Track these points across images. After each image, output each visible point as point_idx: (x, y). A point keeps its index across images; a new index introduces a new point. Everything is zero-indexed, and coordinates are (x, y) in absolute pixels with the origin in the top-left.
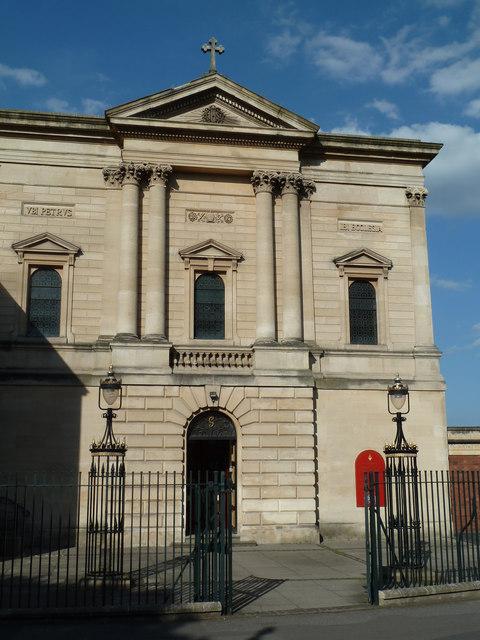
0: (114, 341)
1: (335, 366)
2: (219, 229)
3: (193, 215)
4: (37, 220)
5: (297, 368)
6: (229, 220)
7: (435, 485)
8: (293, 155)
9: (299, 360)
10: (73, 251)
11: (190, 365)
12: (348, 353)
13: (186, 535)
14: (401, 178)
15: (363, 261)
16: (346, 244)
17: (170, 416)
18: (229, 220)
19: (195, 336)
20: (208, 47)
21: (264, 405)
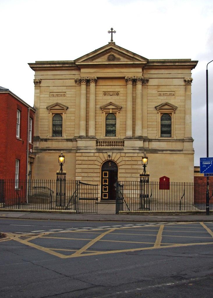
0: (78, 138)
1: (154, 145)
2: (114, 98)
3: (105, 94)
4: (162, 98)
6: (64, 95)
8: (140, 70)
9: (140, 144)
10: (65, 108)
12: (159, 140)
13: (24, 203)
14: (182, 75)
15: (57, 107)
16: (160, 100)
17: (96, 163)
18: (64, 95)
19: (106, 136)
21: (127, 159)
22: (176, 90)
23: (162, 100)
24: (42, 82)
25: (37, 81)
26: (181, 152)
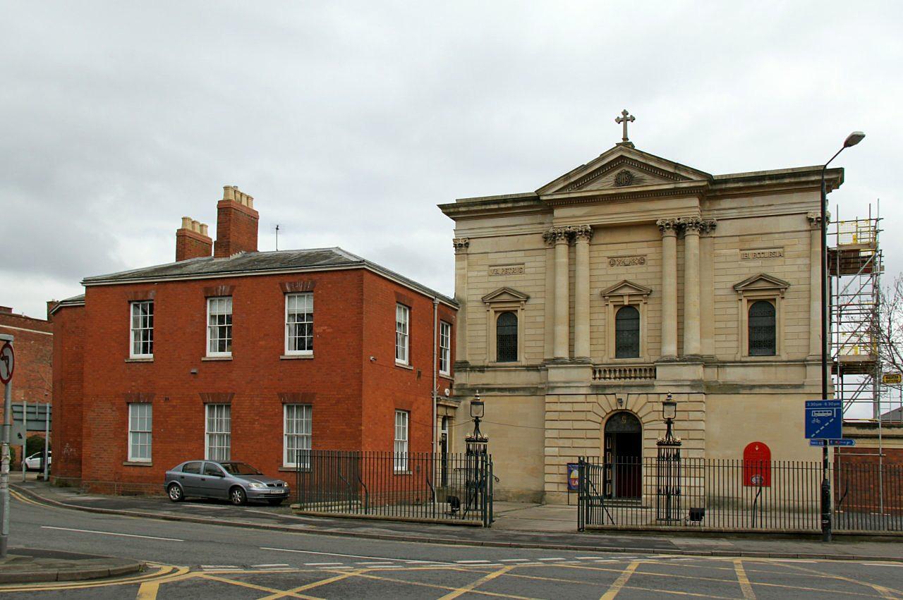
1: (733, 375)
3: (613, 261)
5: (691, 379)
7: (726, 469)
12: (743, 364)
15: (505, 297)
16: (746, 270)
17: (591, 416)
19: (617, 356)
23: (753, 268)
26: (800, 391)
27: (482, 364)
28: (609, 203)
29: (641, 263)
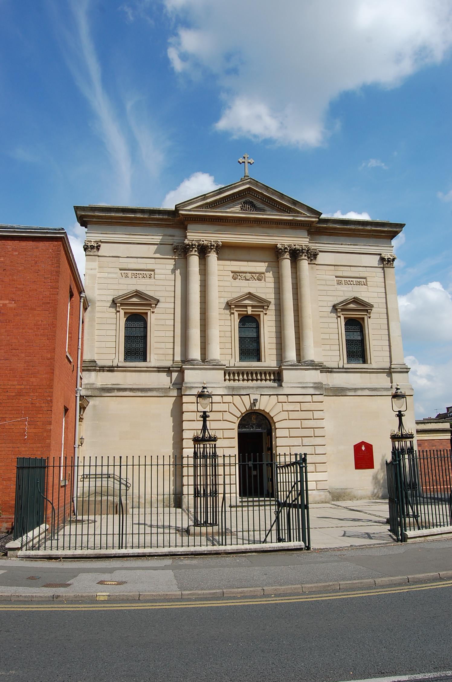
3: (236, 275)
11: (239, 380)
16: (341, 293)
17: (227, 416)
20: (243, 160)
21: (291, 407)
22: (368, 275)
24: (101, 248)
25: (93, 244)
27: (111, 364)
28: (236, 226)
29: (259, 280)
